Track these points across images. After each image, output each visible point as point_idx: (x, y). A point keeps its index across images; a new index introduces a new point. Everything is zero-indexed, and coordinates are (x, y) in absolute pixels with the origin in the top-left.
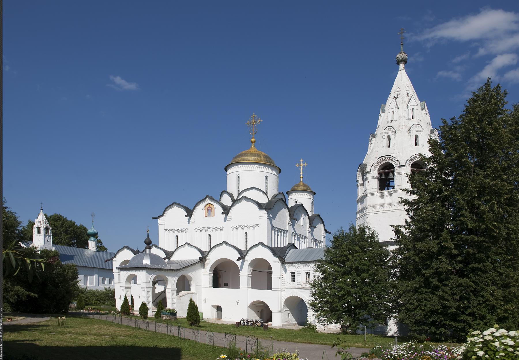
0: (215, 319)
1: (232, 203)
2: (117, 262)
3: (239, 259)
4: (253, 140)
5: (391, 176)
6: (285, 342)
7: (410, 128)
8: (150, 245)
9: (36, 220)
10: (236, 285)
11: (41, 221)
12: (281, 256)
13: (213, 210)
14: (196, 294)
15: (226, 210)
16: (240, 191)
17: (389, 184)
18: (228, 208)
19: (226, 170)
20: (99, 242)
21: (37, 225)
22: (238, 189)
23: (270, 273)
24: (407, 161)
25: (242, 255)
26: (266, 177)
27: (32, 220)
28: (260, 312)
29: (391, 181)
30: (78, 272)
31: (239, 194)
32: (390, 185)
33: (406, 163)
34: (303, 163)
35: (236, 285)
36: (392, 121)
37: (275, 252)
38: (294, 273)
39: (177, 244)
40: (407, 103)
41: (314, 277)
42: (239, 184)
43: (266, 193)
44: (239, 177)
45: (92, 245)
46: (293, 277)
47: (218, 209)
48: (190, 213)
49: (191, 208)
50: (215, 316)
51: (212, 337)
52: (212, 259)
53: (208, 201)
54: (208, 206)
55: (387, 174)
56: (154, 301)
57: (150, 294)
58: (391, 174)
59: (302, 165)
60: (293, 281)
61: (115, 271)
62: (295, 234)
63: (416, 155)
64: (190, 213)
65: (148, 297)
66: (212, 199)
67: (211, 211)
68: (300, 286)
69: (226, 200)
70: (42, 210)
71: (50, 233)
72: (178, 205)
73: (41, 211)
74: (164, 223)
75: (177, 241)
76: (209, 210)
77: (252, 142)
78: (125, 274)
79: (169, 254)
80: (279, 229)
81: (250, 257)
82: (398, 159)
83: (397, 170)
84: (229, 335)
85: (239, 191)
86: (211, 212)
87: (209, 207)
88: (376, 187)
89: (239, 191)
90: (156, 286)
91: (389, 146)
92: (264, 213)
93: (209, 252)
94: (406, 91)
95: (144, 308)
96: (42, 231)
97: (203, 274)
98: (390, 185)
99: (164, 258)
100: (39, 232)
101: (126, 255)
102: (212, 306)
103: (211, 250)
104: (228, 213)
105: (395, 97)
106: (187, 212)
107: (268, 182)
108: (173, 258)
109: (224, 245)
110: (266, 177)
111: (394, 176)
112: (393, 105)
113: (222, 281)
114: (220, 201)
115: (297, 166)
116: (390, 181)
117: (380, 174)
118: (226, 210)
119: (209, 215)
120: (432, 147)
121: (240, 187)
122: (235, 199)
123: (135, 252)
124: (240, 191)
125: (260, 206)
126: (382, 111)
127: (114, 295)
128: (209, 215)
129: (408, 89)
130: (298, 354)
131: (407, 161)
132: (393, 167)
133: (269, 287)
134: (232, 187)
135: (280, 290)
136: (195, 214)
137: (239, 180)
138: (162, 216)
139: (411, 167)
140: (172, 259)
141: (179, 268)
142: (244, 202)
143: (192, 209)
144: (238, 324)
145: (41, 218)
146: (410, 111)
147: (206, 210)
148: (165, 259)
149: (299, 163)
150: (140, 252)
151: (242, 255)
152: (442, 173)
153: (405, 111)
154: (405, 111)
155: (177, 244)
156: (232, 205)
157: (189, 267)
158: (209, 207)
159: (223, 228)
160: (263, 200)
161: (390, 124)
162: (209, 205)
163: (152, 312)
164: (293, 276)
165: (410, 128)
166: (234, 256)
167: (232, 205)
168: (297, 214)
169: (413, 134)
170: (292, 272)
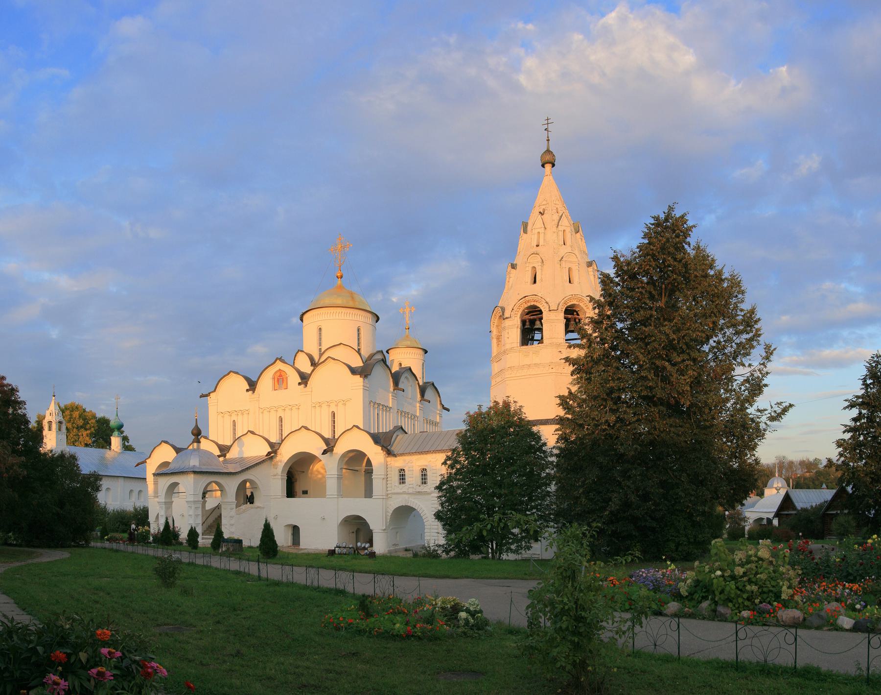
0: (290, 546)
1: (312, 368)
2: (151, 467)
3: (325, 452)
5: (538, 324)
6: (235, 562)
7: (562, 258)
8: (199, 437)
9: (48, 413)
10: (321, 492)
11: (51, 415)
12: (385, 446)
13: (285, 380)
14: (263, 508)
15: (304, 379)
16: (323, 351)
17: (533, 337)
19: (302, 320)
20: (125, 439)
21: (48, 418)
22: (320, 347)
23: (369, 472)
24: (559, 305)
26: (359, 330)
27: (42, 414)
28: (355, 532)
29: (536, 332)
31: (321, 355)
32: (535, 338)
33: (558, 306)
35: (321, 492)
36: (537, 246)
37: (377, 439)
38: (404, 470)
39: (234, 434)
40: (556, 222)
42: (320, 339)
43: (359, 352)
45: (116, 442)
46: (403, 476)
47: (294, 378)
48: (252, 385)
49: (254, 379)
50: (290, 543)
51: (291, 573)
52: (286, 453)
53: (279, 365)
54: (278, 374)
55: (532, 322)
56: (204, 523)
57: (200, 512)
58: (538, 322)
60: (403, 483)
61: (150, 478)
62: (403, 414)
63: (571, 296)
64: (252, 385)
65: (197, 516)
66: (284, 362)
67: (283, 381)
68: (411, 491)
69: (304, 365)
70: (54, 396)
71: (64, 427)
72: (237, 373)
73: (54, 398)
74: (218, 403)
75: (234, 429)
76: (280, 380)
78: (165, 482)
79: (224, 450)
80: (379, 405)
81: (341, 448)
82: (547, 300)
83: (545, 315)
84: (310, 569)
85: (320, 349)
86: (283, 383)
87: (281, 376)
88: (519, 341)
90: (206, 499)
91: (535, 282)
92: (358, 379)
94: (555, 205)
95: (193, 534)
96: (54, 426)
97: (272, 477)
98: (535, 338)
99: (218, 456)
100: (50, 429)
101: (165, 454)
102: (286, 526)
103: (282, 441)
104: (307, 383)
105: (540, 212)
106: (250, 385)
107: (362, 335)
108: (231, 455)
111: (542, 325)
112: (539, 223)
113: (299, 487)
114: (294, 365)
116: (534, 333)
117: (524, 322)
118: (304, 379)
119: (280, 388)
121: (323, 344)
122: (317, 360)
123: (178, 450)
124: (323, 351)
125: (354, 371)
126: (524, 231)
127: (147, 516)
128: (280, 388)
129: (557, 202)
130: (878, 558)
131: (559, 305)
132: (541, 312)
133: (369, 493)
134: (310, 345)
135: (384, 497)
136: (260, 387)
137: (320, 334)
138: (215, 390)
139: (565, 313)
140: (228, 456)
141: (240, 469)
144: (332, 553)
145: (53, 408)
146: (561, 234)
147: (276, 380)
148: (219, 456)
150: (185, 449)
153: (554, 232)
154: (554, 232)
155: (234, 434)
156: (313, 371)
157: (252, 468)
158: (281, 376)
159: (300, 406)
160: (357, 363)
161: (535, 249)
162: (280, 373)
163: (205, 541)
164: (403, 474)
165: (562, 258)
166: (315, 447)
167: (313, 371)
169: (566, 266)
170: (401, 470)
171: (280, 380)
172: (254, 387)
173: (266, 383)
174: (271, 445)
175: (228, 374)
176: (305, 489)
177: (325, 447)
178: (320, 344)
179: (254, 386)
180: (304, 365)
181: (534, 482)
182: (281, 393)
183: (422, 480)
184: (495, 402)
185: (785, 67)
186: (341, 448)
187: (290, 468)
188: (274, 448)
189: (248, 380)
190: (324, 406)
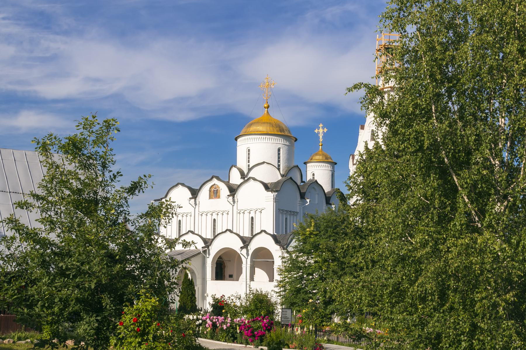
4: (266, 106)
15: (233, 190)
18: (236, 187)
19: (236, 140)
22: (249, 164)
25: (246, 242)
26: (279, 150)
30: (25, 226)
34: (323, 128)
41: (7, 286)
43: (279, 169)
44: (249, 150)
47: (224, 191)
48: (195, 193)
52: (215, 249)
53: (215, 181)
59: (321, 130)
64: (195, 193)
66: (218, 178)
72: (183, 185)
76: (215, 193)
77: (265, 108)
81: (254, 246)
85: (249, 165)
89: (249, 165)
93: (213, 240)
103: (215, 237)
106: (192, 194)
109: (228, 232)
110: (279, 150)
115: (317, 132)
118: (233, 190)
120: (168, 245)
125: (267, 187)
134: (242, 162)
137: (249, 154)
142: (252, 181)
143: (198, 188)
149: (319, 128)
151: (246, 242)
152: (73, 287)
166: (236, 245)
167: (241, 184)
168: (309, 192)
171: (215, 193)
172: (234, 193)
173: (205, 192)
174: (205, 241)
175: (177, 185)
176: (231, 274)
177: (242, 245)
178: (249, 162)
179: (234, 191)
180: (235, 178)
181: (304, 205)
182: (214, 201)
183: (290, 211)
184: (105, 122)
185: (56, 339)
186: (254, 246)
187: (220, 257)
188: (208, 243)
189: (190, 189)
190: (209, 216)
